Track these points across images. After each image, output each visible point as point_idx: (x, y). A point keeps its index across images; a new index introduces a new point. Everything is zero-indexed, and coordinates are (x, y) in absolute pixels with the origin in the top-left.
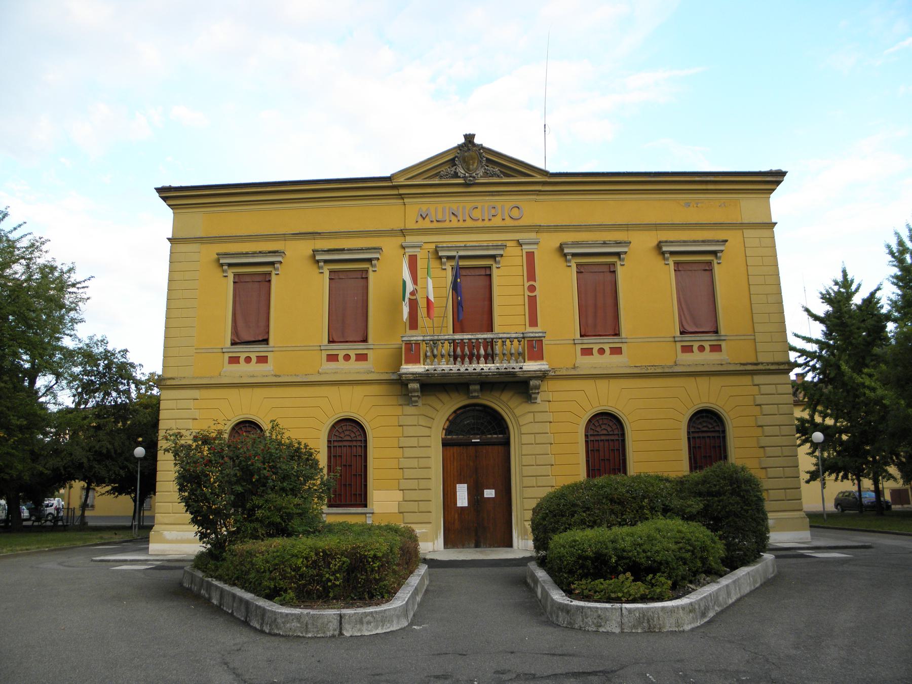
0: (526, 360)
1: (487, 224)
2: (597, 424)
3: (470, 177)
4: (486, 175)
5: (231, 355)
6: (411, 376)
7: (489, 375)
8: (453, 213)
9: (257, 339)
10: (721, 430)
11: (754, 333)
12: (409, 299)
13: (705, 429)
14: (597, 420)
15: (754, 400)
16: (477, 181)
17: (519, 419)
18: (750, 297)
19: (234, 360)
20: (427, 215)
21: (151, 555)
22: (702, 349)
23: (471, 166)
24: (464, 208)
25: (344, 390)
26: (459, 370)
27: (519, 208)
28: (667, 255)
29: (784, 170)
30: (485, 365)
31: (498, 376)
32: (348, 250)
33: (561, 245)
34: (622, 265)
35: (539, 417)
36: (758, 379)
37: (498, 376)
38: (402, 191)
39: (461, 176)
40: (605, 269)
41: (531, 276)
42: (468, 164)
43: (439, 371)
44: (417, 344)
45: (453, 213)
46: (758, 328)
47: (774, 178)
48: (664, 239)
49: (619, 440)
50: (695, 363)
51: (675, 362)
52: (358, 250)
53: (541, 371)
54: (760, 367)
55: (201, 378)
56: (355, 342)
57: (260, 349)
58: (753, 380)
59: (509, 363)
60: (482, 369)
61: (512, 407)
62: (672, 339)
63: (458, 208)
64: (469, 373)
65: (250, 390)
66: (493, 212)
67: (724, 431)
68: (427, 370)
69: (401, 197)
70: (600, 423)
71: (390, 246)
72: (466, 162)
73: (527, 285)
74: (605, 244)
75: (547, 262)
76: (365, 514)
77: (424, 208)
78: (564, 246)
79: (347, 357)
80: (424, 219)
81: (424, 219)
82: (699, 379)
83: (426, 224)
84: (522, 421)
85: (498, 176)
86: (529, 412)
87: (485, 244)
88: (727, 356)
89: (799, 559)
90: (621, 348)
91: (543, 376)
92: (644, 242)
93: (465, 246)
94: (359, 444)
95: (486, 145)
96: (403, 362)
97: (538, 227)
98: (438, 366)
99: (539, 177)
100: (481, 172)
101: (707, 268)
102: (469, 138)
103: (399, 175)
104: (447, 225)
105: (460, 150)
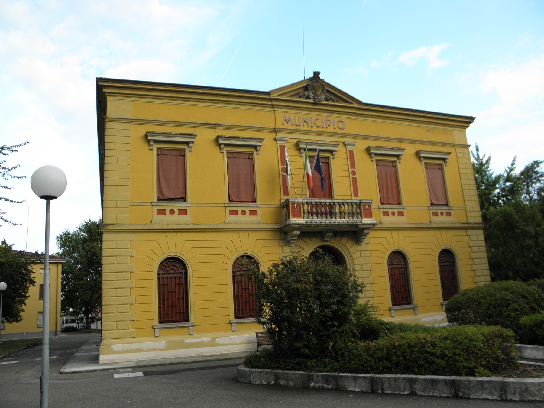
0: (363, 217)
1: (325, 130)
2: (166, 265)
3: (317, 99)
4: (326, 99)
5: (159, 208)
6: (297, 225)
7: (344, 226)
8: (305, 121)
9: (177, 197)
10: (453, 261)
11: (465, 205)
12: (352, 178)
13: (445, 261)
14: (395, 255)
15: (468, 244)
16: (321, 102)
17: (353, 255)
18: (462, 186)
19: (161, 212)
20: (289, 120)
21: (103, 364)
22: (442, 214)
23: (318, 92)
24: (311, 118)
25: (243, 235)
26: (325, 222)
27: (342, 122)
28: (222, 146)
29: (474, 116)
30: (340, 220)
31: (348, 227)
32: (242, 138)
33: (147, 133)
34: (333, 159)
35: (363, 254)
36: (470, 232)
37: (348, 227)
38: (274, 103)
39: (312, 97)
40: (391, 164)
41: (353, 166)
42: (316, 91)
43: (314, 223)
44: (298, 204)
45: (305, 121)
46: (467, 203)
47: (470, 120)
48: (422, 149)
49: (183, 277)
50: (391, 222)
51: (380, 221)
52: (249, 139)
53: (373, 224)
54: (470, 225)
55: (137, 224)
56: (247, 202)
57: (180, 205)
58: (467, 232)
59: (353, 218)
60: (339, 222)
61: (348, 247)
62: (427, 208)
63: (308, 118)
64: (327, 224)
65: (174, 234)
66: (328, 123)
67: (454, 262)
68: (307, 222)
69: (273, 106)
70: (394, 257)
71: (268, 137)
72: (314, 89)
73: (351, 170)
74: (392, 149)
75: (361, 158)
76: (189, 327)
77: (287, 116)
78: (148, 134)
79: (244, 213)
80: (287, 123)
81: (287, 123)
82: (168, 235)
83: (289, 126)
84: (354, 256)
85: (334, 101)
86: (358, 251)
87: (328, 143)
88: (455, 219)
89: (214, 365)
90: (257, 211)
91: (372, 227)
92: (410, 150)
93: (316, 143)
94: (402, 266)
95: (326, 80)
96: (291, 216)
97: (355, 135)
98: (313, 220)
99: (356, 104)
100: (323, 97)
101: (440, 168)
102: (317, 74)
103: (274, 92)
104: (301, 128)
105: (311, 81)
